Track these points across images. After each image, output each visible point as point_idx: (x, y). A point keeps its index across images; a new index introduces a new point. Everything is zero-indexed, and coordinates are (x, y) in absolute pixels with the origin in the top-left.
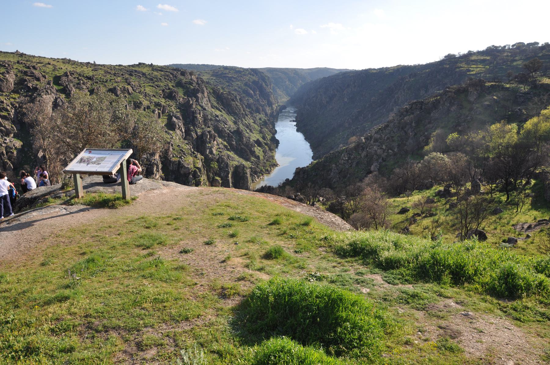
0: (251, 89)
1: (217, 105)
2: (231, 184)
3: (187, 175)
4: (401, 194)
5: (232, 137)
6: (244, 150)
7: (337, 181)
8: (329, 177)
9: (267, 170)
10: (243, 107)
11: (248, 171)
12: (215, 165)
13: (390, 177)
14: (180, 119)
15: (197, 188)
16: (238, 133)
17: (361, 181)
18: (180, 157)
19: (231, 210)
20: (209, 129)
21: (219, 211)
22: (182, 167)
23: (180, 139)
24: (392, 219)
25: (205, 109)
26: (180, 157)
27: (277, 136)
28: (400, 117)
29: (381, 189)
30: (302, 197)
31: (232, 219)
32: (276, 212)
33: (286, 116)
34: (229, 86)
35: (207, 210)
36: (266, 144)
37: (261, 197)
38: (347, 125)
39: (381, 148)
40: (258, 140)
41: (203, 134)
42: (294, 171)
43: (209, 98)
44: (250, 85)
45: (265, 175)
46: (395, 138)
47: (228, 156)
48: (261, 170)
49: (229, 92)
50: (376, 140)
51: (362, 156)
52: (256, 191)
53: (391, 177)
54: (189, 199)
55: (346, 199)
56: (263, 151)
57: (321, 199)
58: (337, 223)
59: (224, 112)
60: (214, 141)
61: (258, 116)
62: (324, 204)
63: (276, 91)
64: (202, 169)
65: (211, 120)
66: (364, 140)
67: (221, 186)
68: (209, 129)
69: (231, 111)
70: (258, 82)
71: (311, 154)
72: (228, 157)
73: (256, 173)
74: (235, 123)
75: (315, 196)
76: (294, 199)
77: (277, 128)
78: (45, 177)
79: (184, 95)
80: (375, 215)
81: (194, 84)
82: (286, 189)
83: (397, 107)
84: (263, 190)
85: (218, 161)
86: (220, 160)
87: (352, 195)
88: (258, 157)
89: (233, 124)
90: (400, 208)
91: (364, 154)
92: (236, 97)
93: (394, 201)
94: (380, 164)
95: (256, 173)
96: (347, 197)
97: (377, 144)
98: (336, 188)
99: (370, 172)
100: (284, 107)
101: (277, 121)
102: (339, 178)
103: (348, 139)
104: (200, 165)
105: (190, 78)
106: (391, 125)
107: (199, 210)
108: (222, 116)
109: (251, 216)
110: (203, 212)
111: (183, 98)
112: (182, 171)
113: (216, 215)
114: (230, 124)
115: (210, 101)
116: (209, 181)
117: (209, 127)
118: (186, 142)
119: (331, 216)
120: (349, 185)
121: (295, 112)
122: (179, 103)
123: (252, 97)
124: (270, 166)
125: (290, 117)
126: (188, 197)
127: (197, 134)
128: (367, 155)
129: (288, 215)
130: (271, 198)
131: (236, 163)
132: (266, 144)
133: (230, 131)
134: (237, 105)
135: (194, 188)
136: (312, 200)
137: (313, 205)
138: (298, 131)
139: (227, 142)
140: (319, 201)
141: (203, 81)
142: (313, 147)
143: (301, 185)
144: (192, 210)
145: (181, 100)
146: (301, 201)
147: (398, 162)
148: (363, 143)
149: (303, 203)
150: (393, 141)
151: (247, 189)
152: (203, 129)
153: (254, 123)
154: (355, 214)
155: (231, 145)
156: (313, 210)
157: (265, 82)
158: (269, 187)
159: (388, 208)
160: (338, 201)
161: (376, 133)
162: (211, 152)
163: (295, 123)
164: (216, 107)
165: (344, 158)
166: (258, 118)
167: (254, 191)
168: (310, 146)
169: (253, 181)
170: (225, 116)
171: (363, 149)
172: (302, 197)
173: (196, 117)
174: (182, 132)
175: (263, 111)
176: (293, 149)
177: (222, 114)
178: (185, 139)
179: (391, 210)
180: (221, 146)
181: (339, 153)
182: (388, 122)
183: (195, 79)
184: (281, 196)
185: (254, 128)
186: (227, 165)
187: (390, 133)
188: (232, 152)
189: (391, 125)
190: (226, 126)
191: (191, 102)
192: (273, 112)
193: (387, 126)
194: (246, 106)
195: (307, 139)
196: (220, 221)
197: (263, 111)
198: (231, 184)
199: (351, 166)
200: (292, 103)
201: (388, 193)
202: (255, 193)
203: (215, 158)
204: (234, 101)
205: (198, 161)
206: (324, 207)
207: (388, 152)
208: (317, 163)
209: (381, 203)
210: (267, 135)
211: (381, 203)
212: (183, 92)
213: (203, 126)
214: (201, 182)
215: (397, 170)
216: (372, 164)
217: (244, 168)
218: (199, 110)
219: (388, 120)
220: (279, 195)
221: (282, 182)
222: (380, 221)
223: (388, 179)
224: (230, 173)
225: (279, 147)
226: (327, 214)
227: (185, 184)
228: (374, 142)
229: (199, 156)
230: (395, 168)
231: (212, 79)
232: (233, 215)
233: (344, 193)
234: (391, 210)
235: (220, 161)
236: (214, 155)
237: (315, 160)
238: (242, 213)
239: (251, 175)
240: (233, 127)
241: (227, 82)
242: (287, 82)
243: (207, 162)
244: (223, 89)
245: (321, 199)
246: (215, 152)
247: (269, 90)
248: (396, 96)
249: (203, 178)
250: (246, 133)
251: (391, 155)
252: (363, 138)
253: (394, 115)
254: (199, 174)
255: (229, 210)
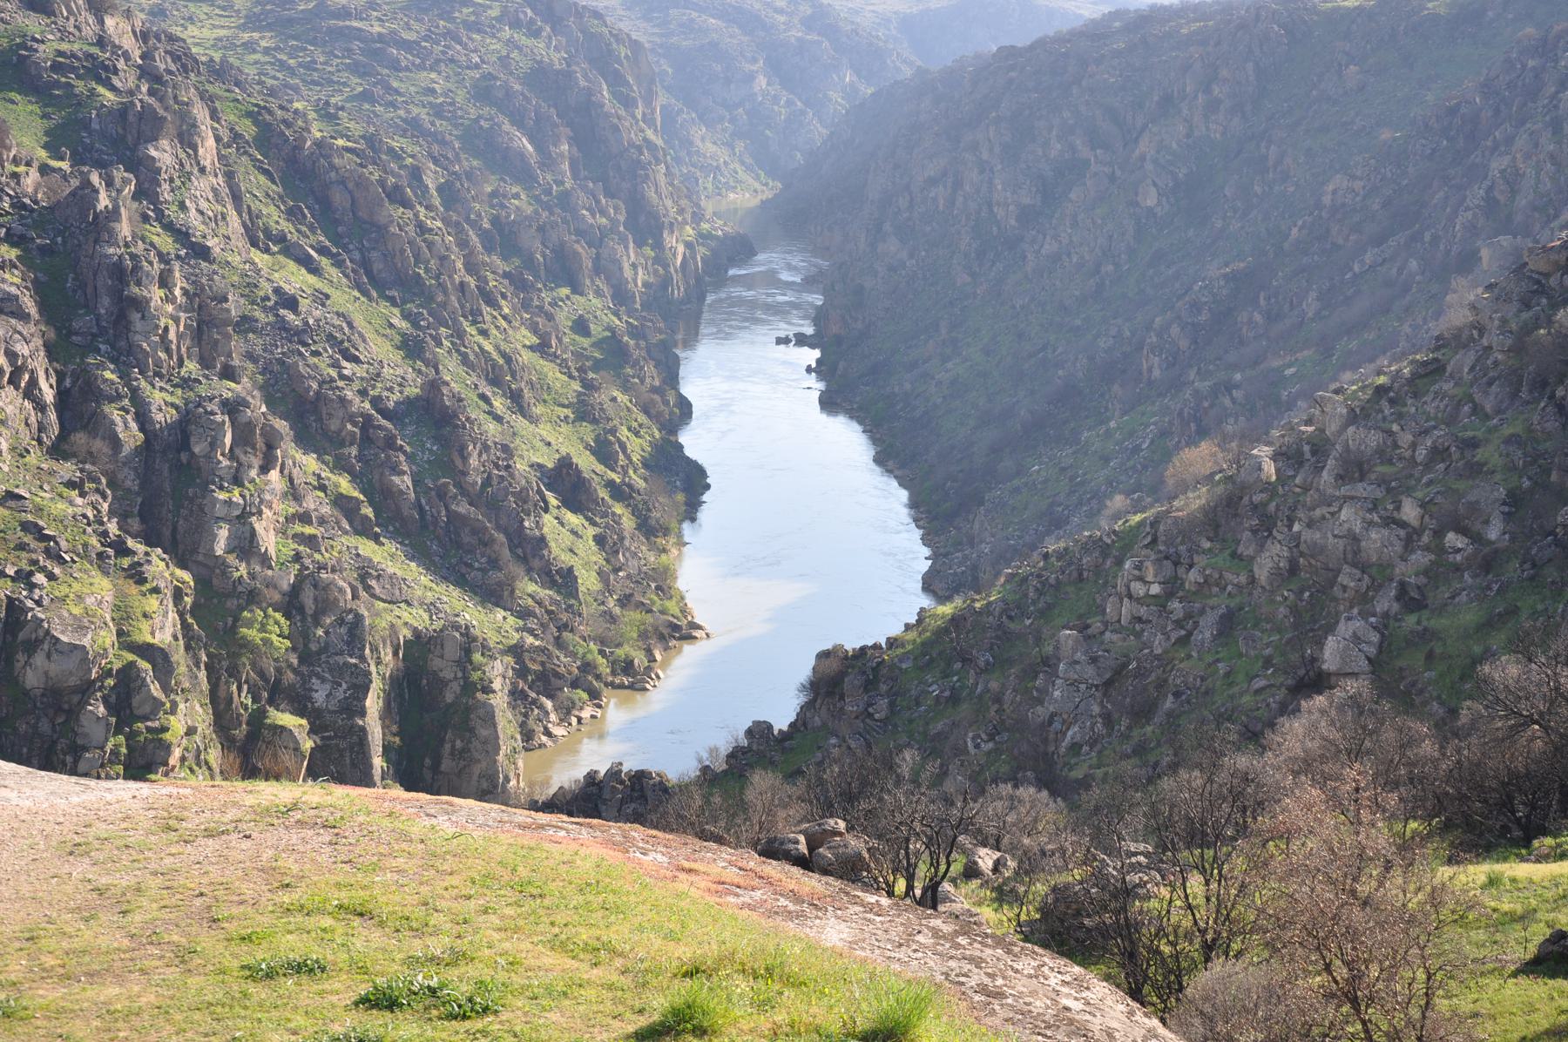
0: (519, 123)
1: (286, 226)
2: (378, 762)
3: (63, 703)
4: (1544, 832)
5: (390, 443)
6: (470, 537)
7: (1093, 743)
8: (1041, 712)
9: (628, 667)
10: (463, 244)
11: (498, 673)
12: (269, 632)
13: (1454, 712)
14: (24, 317)
15: (142, 789)
16: (433, 415)
17: (1254, 736)
18: (24, 577)
19: (377, 937)
20: (228, 389)
21: (292, 946)
22: (32, 646)
23: (20, 453)
24: (1484, 1007)
25: (202, 252)
26: (24, 577)
27: (694, 442)
28: (1527, 305)
29: (1392, 800)
30: (856, 844)
31: (383, 1001)
32: (685, 952)
33: (753, 304)
34: (366, 96)
35: (208, 941)
36: (620, 492)
37: (584, 845)
38: (1154, 366)
39: (1391, 521)
40: (565, 464)
41: (189, 421)
42: (804, 669)
43: (229, 176)
44: (509, 93)
45: (611, 700)
46: (1490, 454)
47: (365, 573)
48: (587, 667)
49: (371, 140)
50: (1356, 468)
51: (1262, 571)
52: (549, 806)
53: (1465, 717)
54: (80, 868)
55: (1155, 863)
56: (600, 540)
57: (986, 859)
58: (1096, 1024)
59: (334, 273)
60: (264, 469)
61: (568, 306)
62: (1003, 895)
63: (687, 143)
64: (180, 657)
65: (245, 324)
66: (1270, 469)
67: (313, 774)
68: (228, 389)
69: (383, 271)
70: (568, 75)
71: (920, 559)
72: (363, 577)
73: (547, 682)
74: (412, 348)
75: (943, 842)
76: (804, 863)
77: (690, 388)
78: (1106, 774)
79: (53, 148)
80: (1356, 978)
81: (126, 78)
82: (750, 795)
83: (1505, 241)
84: (594, 800)
85: (291, 605)
86: (308, 598)
87: (1197, 836)
88: (564, 581)
89: (397, 356)
90: (1539, 933)
91: (1269, 560)
92: (416, 174)
93: (1493, 882)
94: (1384, 625)
95: (540, 682)
96: (1163, 847)
97: (1362, 489)
98: (1085, 783)
99: (1317, 682)
100: (739, 249)
101: (691, 341)
102: (1108, 719)
103: (1167, 456)
104: (162, 626)
105: (90, 31)
106: (1462, 362)
107: (154, 940)
108: (322, 298)
109: (518, 980)
110: (183, 956)
111: (44, 170)
112: (34, 673)
113: (270, 975)
114: (375, 352)
115: (237, 198)
116: (227, 742)
117: (229, 374)
118: (68, 470)
119: (1054, 980)
120: (1174, 768)
121: (809, 283)
122: (18, 205)
123: (525, 176)
124: (643, 635)
125: (779, 311)
126: (75, 850)
127: (143, 418)
128: (1293, 569)
129: (770, 973)
130: (642, 857)
131: (417, 618)
132: (620, 492)
133: (376, 402)
134: (422, 228)
135: (121, 793)
136: (922, 870)
137: (931, 899)
138: (829, 403)
139: (355, 478)
140: (971, 872)
141: (184, 61)
142: (935, 514)
143: (851, 771)
144: (104, 942)
145: (31, 179)
146: (850, 870)
147: (1513, 611)
148: (1269, 488)
149: (867, 887)
150: (1476, 470)
151: (490, 790)
152: (187, 383)
153: (542, 348)
154: (1218, 966)
155: (381, 495)
156: (936, 933)
157: (616, 80)
158: (640, 776)
159: (1450, 932)
160: (1099, 877)
161: (1353, 418)
162: (246, 545)
163: (812, 356)
164: (281, 239)
165: (1138, 589)
166: (564, 317)
167: (535, 806)
168: (914, 504)
169: (528, 736)
170: (344, 298)
171: (1266, 527)
172: (856, 844)
173: (141, 305)
174: (40, 407)
175: (597, 270)
176: (796, 535)
177: (326, 293)
178: (58, 451)
179: (1471, 942)
180: (314, 502)
181: (1105, 550)
182: (1440, 343)
183: (128, 42)
184: (719, 840)
185: (541, 387)
186: (355, 632)
187: (1451, 421)
188: (390, 546)
189: (1462, 362)
190: (348, 368)
191: (103, 201)
192: (666, 282)
193: (1432, 371)
194: (485, 236)
195: (889, 457)
196: (299, 1021)
197: (597, 270)
198: (378, 762)
199: (1184, 641)
200: (792, 218)
201: (1447, 827)
202: (543, 818)
203: (271, 584)
204: (406, 204)
205: (152, 603)
206: (1009, 912)
207: (1440, 550)
208: (955, 621)
209: (1402, 891)
210: (624, 433)
211: (1402, 891)
212: (40, 126)
213: (191, 367)
214: (167, 748)
215: (1507, 670)
216: (1330, 629)
217: (468, 652)
218: (163, 257)
219: (1437, 328)
220: (703, 836)
221: (725, 748)
222: (1399, 1020)
223: (1446, 729)
224: (376, 686)
225: (704, 514)
226: (1027, 965)
227: (48, 762)
228: (1341, 478)
229: (159, 566)
230: (1488, 655)
231: (250, 47)
232: (390, 973)
233: (1137, 818)
234: (1471, 942)
235: (304, 602)
236: (265, 560)
237: (942, 599)
238: (457, 958)
239: (516, 695)
240: (400, 378)
241: (356, 69)
242: (761, 81)
243: (215, 610)
244: (328, 114)
245: (986, 859)
246: (269, 540)
247: (639, 129)
248: (1497, 164)
249: (187, 718)
250: (486, 423)
251: (1457, 568)
252: (1263, 452)
253: (1478, 293)
254: (155, 690)
255: (366, 940)
